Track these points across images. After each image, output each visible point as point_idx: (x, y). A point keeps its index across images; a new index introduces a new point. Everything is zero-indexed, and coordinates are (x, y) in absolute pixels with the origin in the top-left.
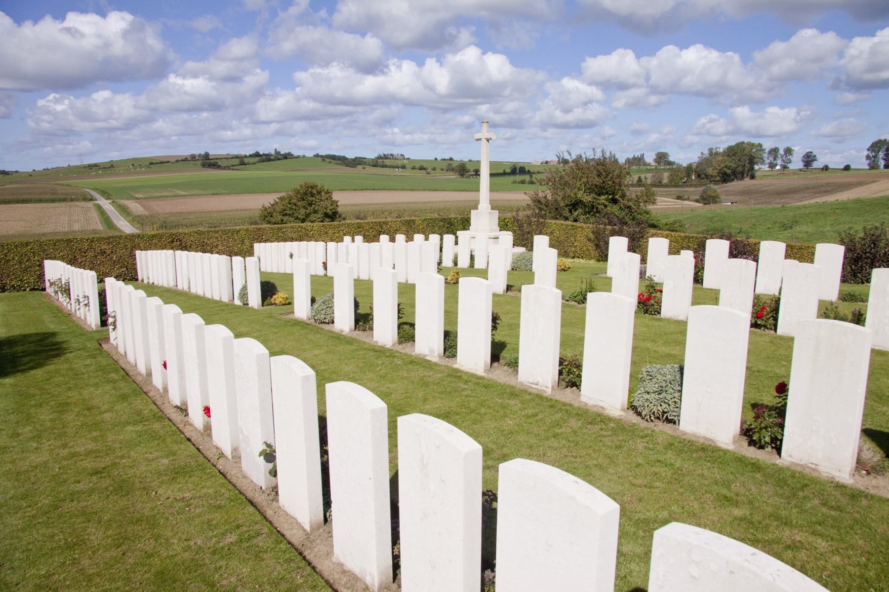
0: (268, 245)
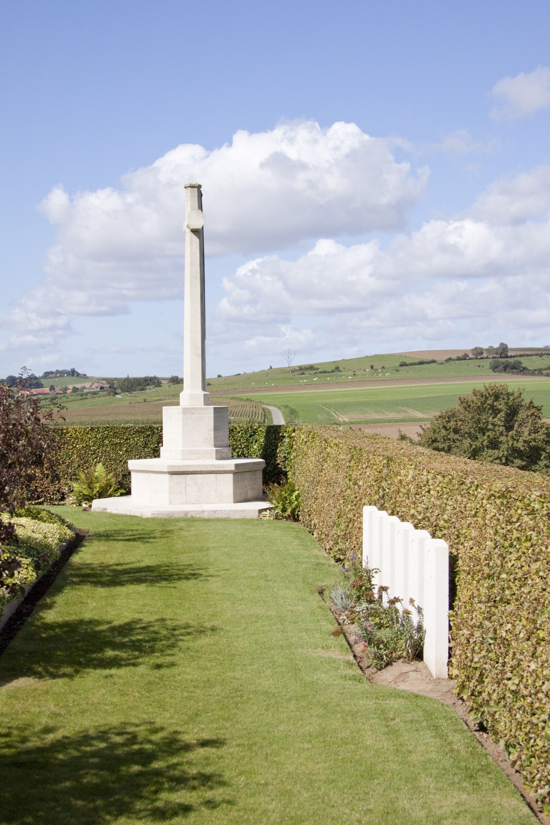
0: (213, 421)
